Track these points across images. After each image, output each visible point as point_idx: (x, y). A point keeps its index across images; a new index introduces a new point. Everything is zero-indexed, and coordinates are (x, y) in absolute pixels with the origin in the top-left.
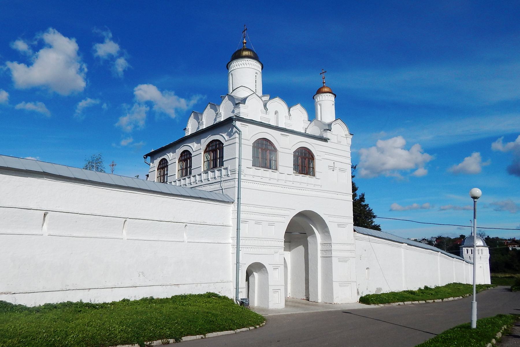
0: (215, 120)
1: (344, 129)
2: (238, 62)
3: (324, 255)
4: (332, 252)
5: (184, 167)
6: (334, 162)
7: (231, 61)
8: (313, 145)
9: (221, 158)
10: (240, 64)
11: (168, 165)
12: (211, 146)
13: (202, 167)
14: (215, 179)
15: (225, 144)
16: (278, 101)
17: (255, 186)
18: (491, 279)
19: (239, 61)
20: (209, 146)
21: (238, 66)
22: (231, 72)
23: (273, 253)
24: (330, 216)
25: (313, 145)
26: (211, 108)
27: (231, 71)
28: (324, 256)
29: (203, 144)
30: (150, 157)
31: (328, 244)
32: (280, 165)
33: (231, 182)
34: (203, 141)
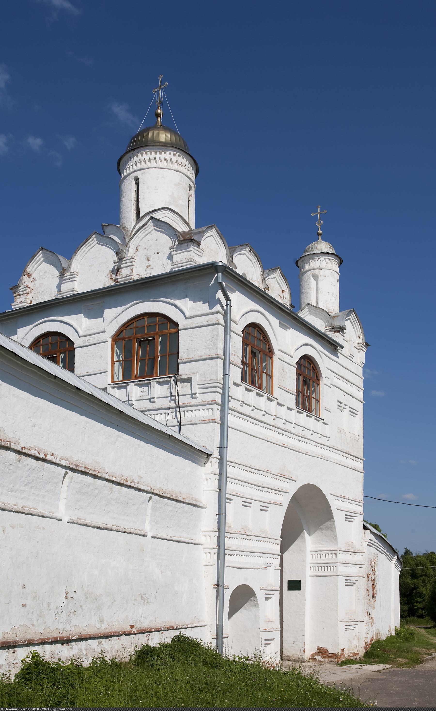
0: (116, 271)
2: (149, 153)
3: (323, 572)
4: (337, 568)
5: (354, 314)
6: (345, 394)
7: (126, 153)
8: (321, 353)
9: (168, 357)
10: (158, 159)
11: (74, 349)
12: (135, 327)
14: (151, 402)
15: (77, 342)
16: (247, 254)
17: (259, 430)
18: (401, 603)
19: (146, 153)
20: (38, 344)
21: (138, 164)
22: (138, 174)
25: (321, 353)
26: (47, 261)
27: (135, 171)
28: (318, 574)
29: (108, 322)
31: (329, 552)
32: (220, 395)
33: (201, 410)
34: (109, 313)
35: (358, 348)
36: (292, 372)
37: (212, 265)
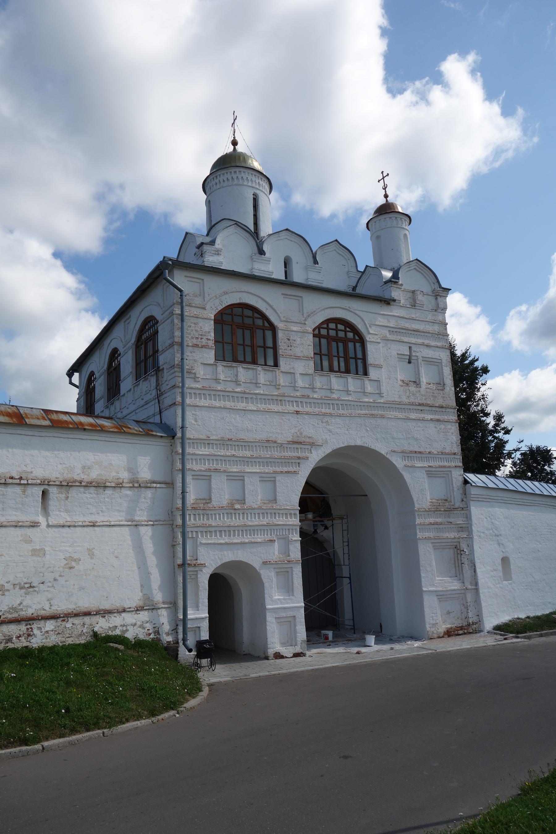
1: (428, 278)
10: (221, 181)
23: (379, 341)
24: (408, 454)
30: (517, 371)
35: (434, 295)
36: (209, 327)
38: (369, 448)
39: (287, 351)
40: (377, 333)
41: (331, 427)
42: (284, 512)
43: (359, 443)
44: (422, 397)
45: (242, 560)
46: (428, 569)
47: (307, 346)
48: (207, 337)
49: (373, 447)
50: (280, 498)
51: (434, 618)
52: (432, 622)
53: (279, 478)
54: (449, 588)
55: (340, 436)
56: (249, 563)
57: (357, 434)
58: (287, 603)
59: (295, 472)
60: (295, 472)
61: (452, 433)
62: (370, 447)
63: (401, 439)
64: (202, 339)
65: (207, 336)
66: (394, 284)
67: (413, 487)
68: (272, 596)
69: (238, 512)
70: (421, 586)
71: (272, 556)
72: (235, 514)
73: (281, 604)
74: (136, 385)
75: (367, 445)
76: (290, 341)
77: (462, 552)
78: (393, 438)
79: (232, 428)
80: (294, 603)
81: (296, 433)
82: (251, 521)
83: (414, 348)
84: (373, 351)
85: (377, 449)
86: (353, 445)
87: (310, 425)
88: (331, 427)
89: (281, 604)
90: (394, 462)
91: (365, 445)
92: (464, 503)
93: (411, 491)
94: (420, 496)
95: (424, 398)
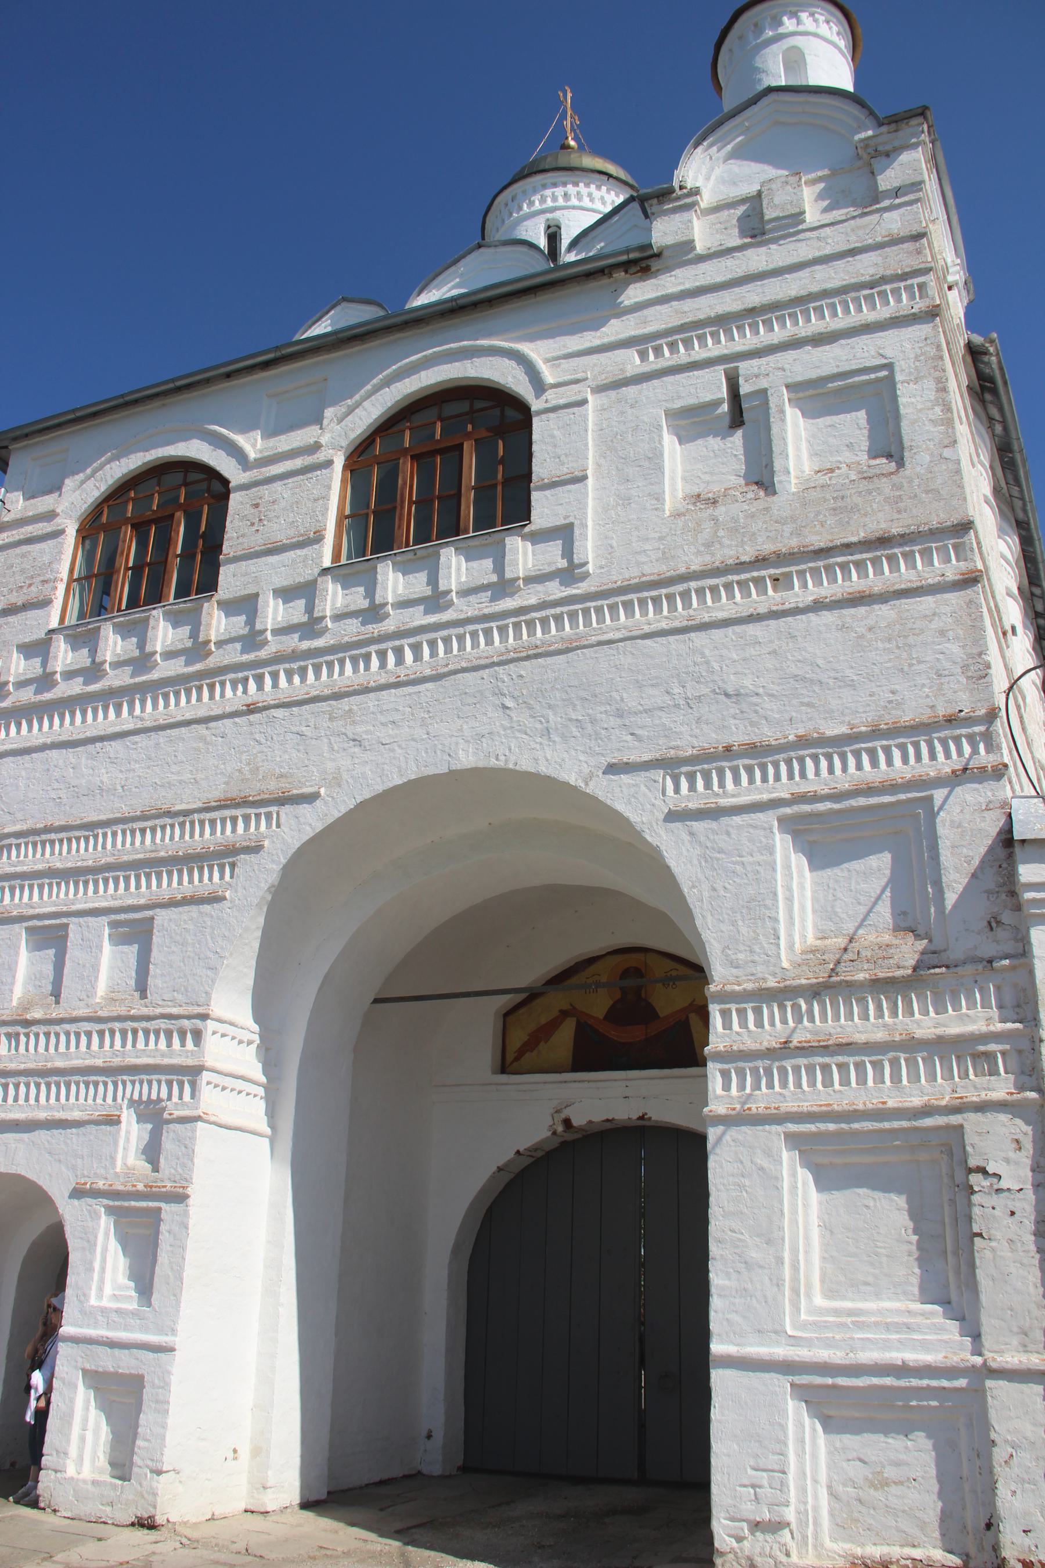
13: (978, 524)
37: (884, 373)
38: (511, 770)
39: (245, 540)
40: (579, 376)
41: (360, 729)
42: (163, 1026)
43: (467, 758)
44: (778, 526)
45: (23, 1173)
46: (754, 1254)
47: (310, 504)
48: (42, 578)
49: (525, 764)
50: (159, 982)
51: (766, 1492)
52: (748, 1509)
53: (162, 917)
54: (868, 1356)
55: (393, 750)
56: (40, 1183)
57: (461, 730)
58: (126, 1328)
59: (215, 899)
60: (215, 899)
61: (942, 633)
62: (511, 766)
63: (661, 709)
64: (30, 585)
65: (44, 575)
66: (660, 203)
67: (706, 894)
68: (85, 1295)
69: (34, 1029)
70: (704, 1335)
71: (105, 1168)
72: (27, 1035)
73: (108, 1326)
74: (995, 1240)
75: (501, 764)
76: (261, 508)
77: (975, 1179)
78: (620, 714)
79: (63, 794)
80: (146, 1330)
81: (240, 771)
82: (66, 1056)
83: (745, 367)
84: (553, 436)
85: (543, 769)
86: (443, 769)
87: (290, 736)
88: (360, 729)
89: (108, 1328)
90: (620, 807)
91: (493, 762)
92: (1001, 933)
93: (697, 912)
94: (744, 930)
95: (788, 529)
